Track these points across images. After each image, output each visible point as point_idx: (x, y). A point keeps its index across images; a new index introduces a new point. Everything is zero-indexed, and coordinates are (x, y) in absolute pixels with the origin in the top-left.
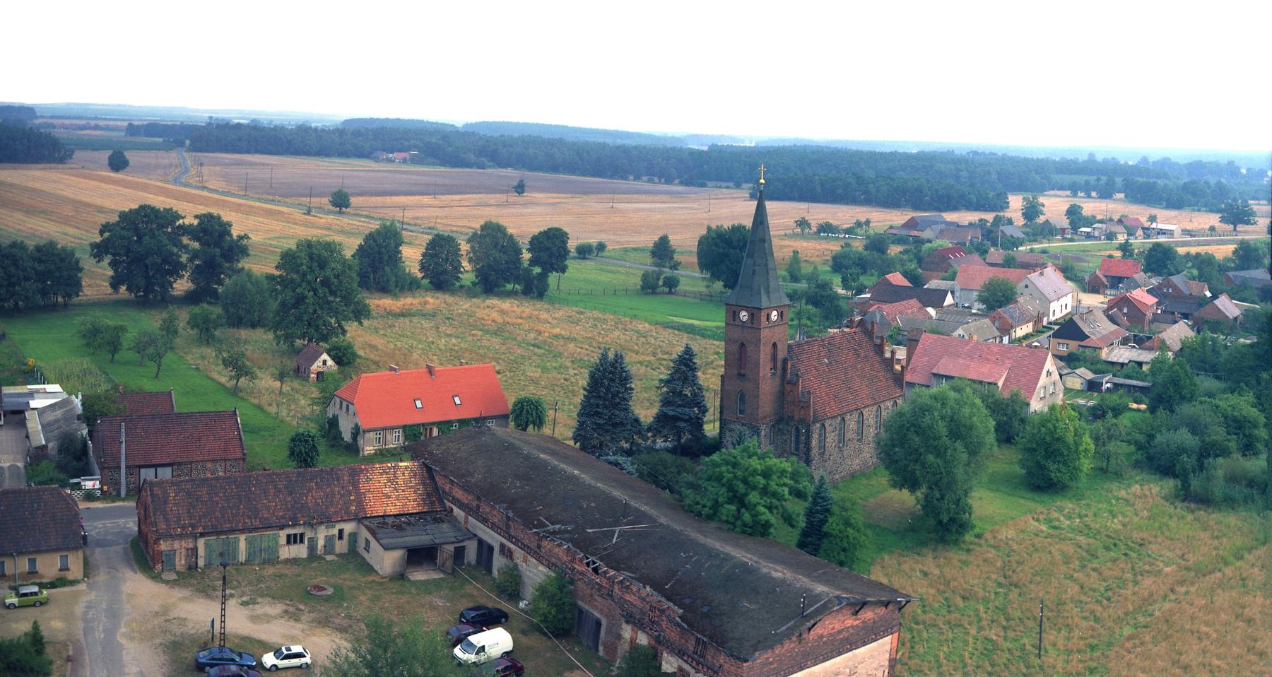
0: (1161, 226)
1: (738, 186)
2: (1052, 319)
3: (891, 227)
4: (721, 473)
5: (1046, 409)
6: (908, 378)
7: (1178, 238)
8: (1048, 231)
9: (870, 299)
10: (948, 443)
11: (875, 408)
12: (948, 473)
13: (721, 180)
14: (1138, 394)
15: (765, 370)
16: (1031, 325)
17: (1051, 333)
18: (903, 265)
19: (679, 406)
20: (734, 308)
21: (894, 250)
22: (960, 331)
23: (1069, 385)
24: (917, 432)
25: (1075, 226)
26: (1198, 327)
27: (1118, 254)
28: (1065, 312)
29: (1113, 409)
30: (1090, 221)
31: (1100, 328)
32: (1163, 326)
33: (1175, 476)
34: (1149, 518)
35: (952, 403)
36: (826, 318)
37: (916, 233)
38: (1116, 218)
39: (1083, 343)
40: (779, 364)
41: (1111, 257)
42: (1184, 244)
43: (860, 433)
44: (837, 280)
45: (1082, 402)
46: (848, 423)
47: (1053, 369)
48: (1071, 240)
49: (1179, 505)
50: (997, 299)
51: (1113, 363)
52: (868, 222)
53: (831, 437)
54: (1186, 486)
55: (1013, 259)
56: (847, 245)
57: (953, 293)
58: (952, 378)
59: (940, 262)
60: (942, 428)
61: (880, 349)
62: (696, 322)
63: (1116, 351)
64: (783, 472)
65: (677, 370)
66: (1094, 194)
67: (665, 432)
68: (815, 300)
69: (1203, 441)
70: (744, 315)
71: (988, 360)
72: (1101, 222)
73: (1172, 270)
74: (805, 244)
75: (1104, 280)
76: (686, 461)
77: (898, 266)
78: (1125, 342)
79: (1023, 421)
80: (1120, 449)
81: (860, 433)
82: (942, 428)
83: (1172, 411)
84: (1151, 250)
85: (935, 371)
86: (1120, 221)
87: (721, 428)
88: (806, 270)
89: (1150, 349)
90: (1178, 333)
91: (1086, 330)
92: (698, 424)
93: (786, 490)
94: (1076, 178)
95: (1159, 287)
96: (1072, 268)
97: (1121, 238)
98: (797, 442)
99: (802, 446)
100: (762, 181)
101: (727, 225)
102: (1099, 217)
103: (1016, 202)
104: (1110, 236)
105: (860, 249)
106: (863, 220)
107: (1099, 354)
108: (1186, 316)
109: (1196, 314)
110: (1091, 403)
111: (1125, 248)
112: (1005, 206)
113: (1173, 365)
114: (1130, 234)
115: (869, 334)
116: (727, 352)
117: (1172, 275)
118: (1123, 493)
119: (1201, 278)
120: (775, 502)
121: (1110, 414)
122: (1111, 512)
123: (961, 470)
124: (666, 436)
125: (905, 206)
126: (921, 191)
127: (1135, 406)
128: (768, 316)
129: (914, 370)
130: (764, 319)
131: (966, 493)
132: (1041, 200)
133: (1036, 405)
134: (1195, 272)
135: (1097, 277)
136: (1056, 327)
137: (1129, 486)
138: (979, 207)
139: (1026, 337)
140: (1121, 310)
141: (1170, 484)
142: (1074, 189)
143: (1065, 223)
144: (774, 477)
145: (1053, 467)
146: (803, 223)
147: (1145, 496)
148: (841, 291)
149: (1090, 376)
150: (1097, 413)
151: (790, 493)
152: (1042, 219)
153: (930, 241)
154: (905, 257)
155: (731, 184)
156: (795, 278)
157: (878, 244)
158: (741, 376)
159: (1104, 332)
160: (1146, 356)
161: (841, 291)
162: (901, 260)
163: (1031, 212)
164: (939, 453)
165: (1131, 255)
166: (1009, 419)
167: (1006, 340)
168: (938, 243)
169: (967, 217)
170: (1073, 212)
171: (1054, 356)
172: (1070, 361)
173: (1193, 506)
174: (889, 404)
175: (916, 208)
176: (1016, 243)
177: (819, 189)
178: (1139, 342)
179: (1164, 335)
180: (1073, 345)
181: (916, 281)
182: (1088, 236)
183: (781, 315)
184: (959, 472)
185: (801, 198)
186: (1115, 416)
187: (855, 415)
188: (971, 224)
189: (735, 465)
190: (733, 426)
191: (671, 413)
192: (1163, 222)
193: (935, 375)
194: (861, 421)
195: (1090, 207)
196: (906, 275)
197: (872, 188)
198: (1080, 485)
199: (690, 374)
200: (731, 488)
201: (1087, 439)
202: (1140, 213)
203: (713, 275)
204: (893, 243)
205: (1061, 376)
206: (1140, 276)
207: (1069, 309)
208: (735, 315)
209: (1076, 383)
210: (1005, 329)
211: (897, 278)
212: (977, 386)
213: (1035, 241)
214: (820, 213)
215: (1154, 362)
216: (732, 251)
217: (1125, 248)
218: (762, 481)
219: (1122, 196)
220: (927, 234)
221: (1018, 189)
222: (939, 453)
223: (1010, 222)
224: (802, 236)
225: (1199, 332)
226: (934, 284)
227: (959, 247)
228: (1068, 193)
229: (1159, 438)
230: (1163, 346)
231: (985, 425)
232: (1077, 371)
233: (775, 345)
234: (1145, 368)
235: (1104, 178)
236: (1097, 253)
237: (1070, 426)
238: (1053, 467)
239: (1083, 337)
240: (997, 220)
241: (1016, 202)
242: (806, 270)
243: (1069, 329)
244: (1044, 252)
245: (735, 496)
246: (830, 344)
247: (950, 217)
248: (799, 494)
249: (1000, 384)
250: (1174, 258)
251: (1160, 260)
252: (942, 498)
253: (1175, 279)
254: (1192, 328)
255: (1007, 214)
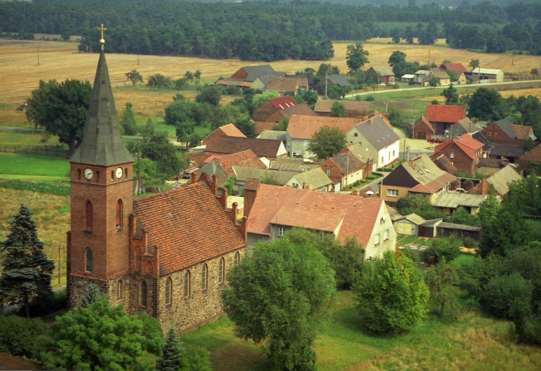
0: (483, 71)
1: (66, 38)
2: (381, 165)
3: (221, 79)
4: (74, 331)
5: (382, 257)
6: (249, 229)
7: (500, 80)
8: (373, 79)
9: (205, 151)
10: (292, 293)
11: (218, 260)
12: (292, 322)
13: (48, 32)
14: (468, 239)
15: (111, 227)
16: (361, 172)
17: (381, 179)
18: (235, 116)
19: (22, 267)
20: (78, 167)
21: (226, 101)
22: (293, 181)
23: (401, 231)
24: (262, 285)
25: (398, 75)
26: (525, 169)
27: (442, 99)
28: (393, 158)
29: (444, 253)
30: (413, 68)
31: (427, 173)
32: (489, 170)
33: (510, 319)
34: (485, 361)
35: (294, 256)
36: (163, 170)
37: (246, 84)
38: (439, 63)
39: (413, 189)
40: (126, 221)
41: (435, 102)
42: (506, 88)
43: (205, 285)
44: (172, 131)
45: (414, 247)
46: (193, 275)
47: (387, 217)
48: (395, 87)
49: (514, 347)
50: (329, 149)
51: (442, 208)
52: (198, 74)
53: (178, 290)
54: (519, 329)
55: (341, 107)
56: (180, 97)
57: (285, 143)
58: (289, 227)
59: (271, 112)
60: (286, 279)
61: (222, 201)
62: (21, 177)
63: (444, 196)
64: (135, 329)
65: (15, 232)
66: (415, 40)
67: (12, 294)
68: (150, 154)
69: (536, 285)
70: (89, 173)
71: (323, 209)
72: (424, 68)
73: (497, 114)
74: (137, 96)
75: (430, 126)
76: (38, 322)
77: (231, 118)
78: (453, 187)
79: (358, 268)
80: (449, 292)
81: (205, 285)
82: (286, 279)
83: (504, 255)
84: (475, 95)
85: (273, 221)
86: (443, 67)
87: (69, 284)
88: (141, 123)
89: (479, 193)
90: (505, 178)
91: (415, 176)
92: (44, 282)
93: (139, 345)
94: (397, 25)
95: (485, 132)
96: (398, 115)
97: (445, 84)
98: (145, 295)
99: (149, 299)
100: (103, 41)
101: (61, 80)
102: (422, 64)
103: (341, 50)
104: (434, 82)
105: (192, 100)
106: (193, 71)
107: (428, 200)
108: (512, 160)
109: (522, 158)
110: (423, 248)
111: (449, 94)
112: (330, 55)
113: (502, 211)
114: (453, 79)
115: (211, 186)
116: (73, 212)
117: (496, 119)
118: (458, 337)
119: (526, 121)
120: (129, 358)
121: (444, 259)
122: (447, 355)
123: (305, 320)
124: (13, 299)
125: (233, 57)
126: (248, 42)
127: (465, 250)
128: (113, 174)
129: (253, 221)
130: (109, 176)
131: (310, 342)
132: (366, 48)
133: (372, 252)
134: (519, 115)
135: (423, 123)
136: (386, 174)
137: (464, 330)
138: (305, 57)
139: (356, 184)
140: (448, 155)
141: (504, 326)
142: (396, 36)
143: (387, 70)
144: (126, 334)
145: (390, 312)
146: (134, 76)
147: (481, 339)
148: (176, 143)
149: (420, 221)
150: (430, 259)
151: (143, 349)
152: (366, 67)
153: (259, 92)
154: (237, 108)
155: (58, 37)
156: (129, 131)
157: (209, 96)
158: (88, 233)
159: (433, 178)
160: (473, 200)
161: (176, 143)
162: (233, 111)
163: (356, 60)
164: (282, 303)
165: (455, 101)
166: (347, 263)
167: (337, 187)
168: (266, 94)
169: (294, 66)
170: (396, 60)
171: (387, 203)
172: (400, 207)
173: (528, 348)
174: (232, 255)
175: (244, 58)
176: (341, 91)
177: (148, 42)
178: (466, 186)
179: (491, 180)
180: (403, 191)
181: (248, 130)
182: (412, 82)
183: (126, 172)
184: (303, 321)
185: (130, 50)
186: (448, 260)
187: (200, 267)
188: (298, 74)
189: (87, 324)
190: (80, 283)
191: (15, 275)
192: (485, 67)
193: (273, 225)
194: (205, 274)
195: (414, 53)
196: (238, 125)
197: (200, 39)
198: (416, 328)
199: (29, 233)
200: (84, 346)
201: (422, 284)
202: (463, 58)
203: (48, 129)
204: (224, 93)
205: (393, 222)
206: (465, 122)
207: (397, 156)
208: (80, 172)
209: (407, 229)
210: (336, 178)
211: (230, 130)
212: (314, 235)
213: (360, 88)
214: (150, 65)
215: (483, 205)
216: (67, 106)
217: (449, 94)
218: (115, 338)
219: (442, 41)
220: (257, 85)
221: (343, 37)
222: (282, 303)
223: (336, 71)
224: (133, 88)
225: (525, 175)
226: (267, 134)
227: (288, 96)
228: (390, 39)
229: (493, 282)
230: (491, 190)
231: (327, 277)
232: (409, 217)
233: (120, 201)
234: (474, 212)
235: (425, 25)
236: (421, 98)
237: (408, 274)
238: (390, 312)
239: (413, 183)
240: (323, 69)
241: (341, 50)
242: (141, 123)
243: (398, 176)
244: (369, 99)
245: (88, 353)
246: (172, 197)
247: (278, 66)
248: (151, 349)
249: (336, 232)
250: (499, 103)
251: (483, 104)
252: (287, 346)
253: (501, 124)
254: (518, 170)
255: (332, 63)
